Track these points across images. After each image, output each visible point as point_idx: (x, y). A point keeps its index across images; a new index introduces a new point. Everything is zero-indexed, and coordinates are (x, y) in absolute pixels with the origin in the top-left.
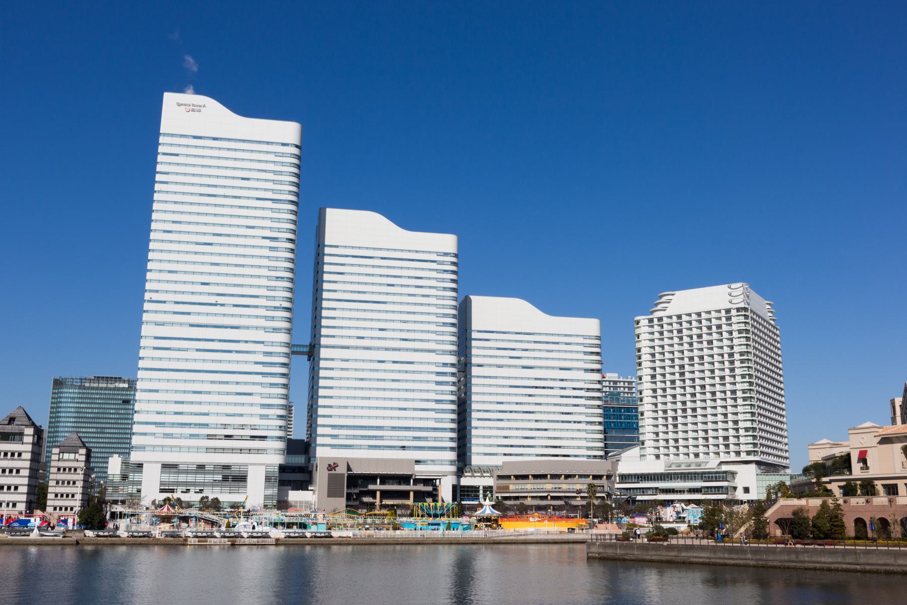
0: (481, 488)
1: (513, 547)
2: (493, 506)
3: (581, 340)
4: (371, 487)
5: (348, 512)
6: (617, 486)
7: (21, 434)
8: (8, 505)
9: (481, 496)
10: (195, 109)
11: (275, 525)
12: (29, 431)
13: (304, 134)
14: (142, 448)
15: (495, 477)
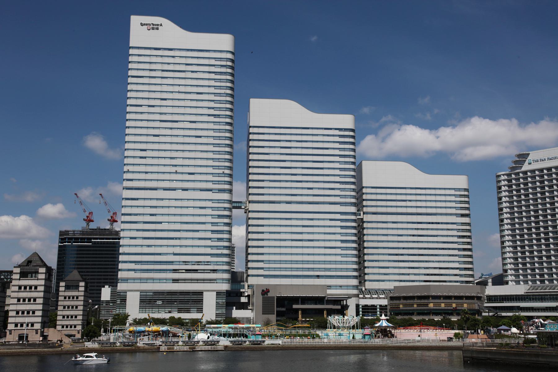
0: (275, 298)
1: (403, 352)
2: (387, 320)
3: (453, 192)
4: (295, 306)
5: (278, 325)
6: (486, 305)
7: (37, 272)
8: (28, 325)
9: (378, 313)
10: (155, 27)
11: (225, 335)
12: (42, 270)
13: (236, 43)
14: (126, 280)
15: (389, 298)
